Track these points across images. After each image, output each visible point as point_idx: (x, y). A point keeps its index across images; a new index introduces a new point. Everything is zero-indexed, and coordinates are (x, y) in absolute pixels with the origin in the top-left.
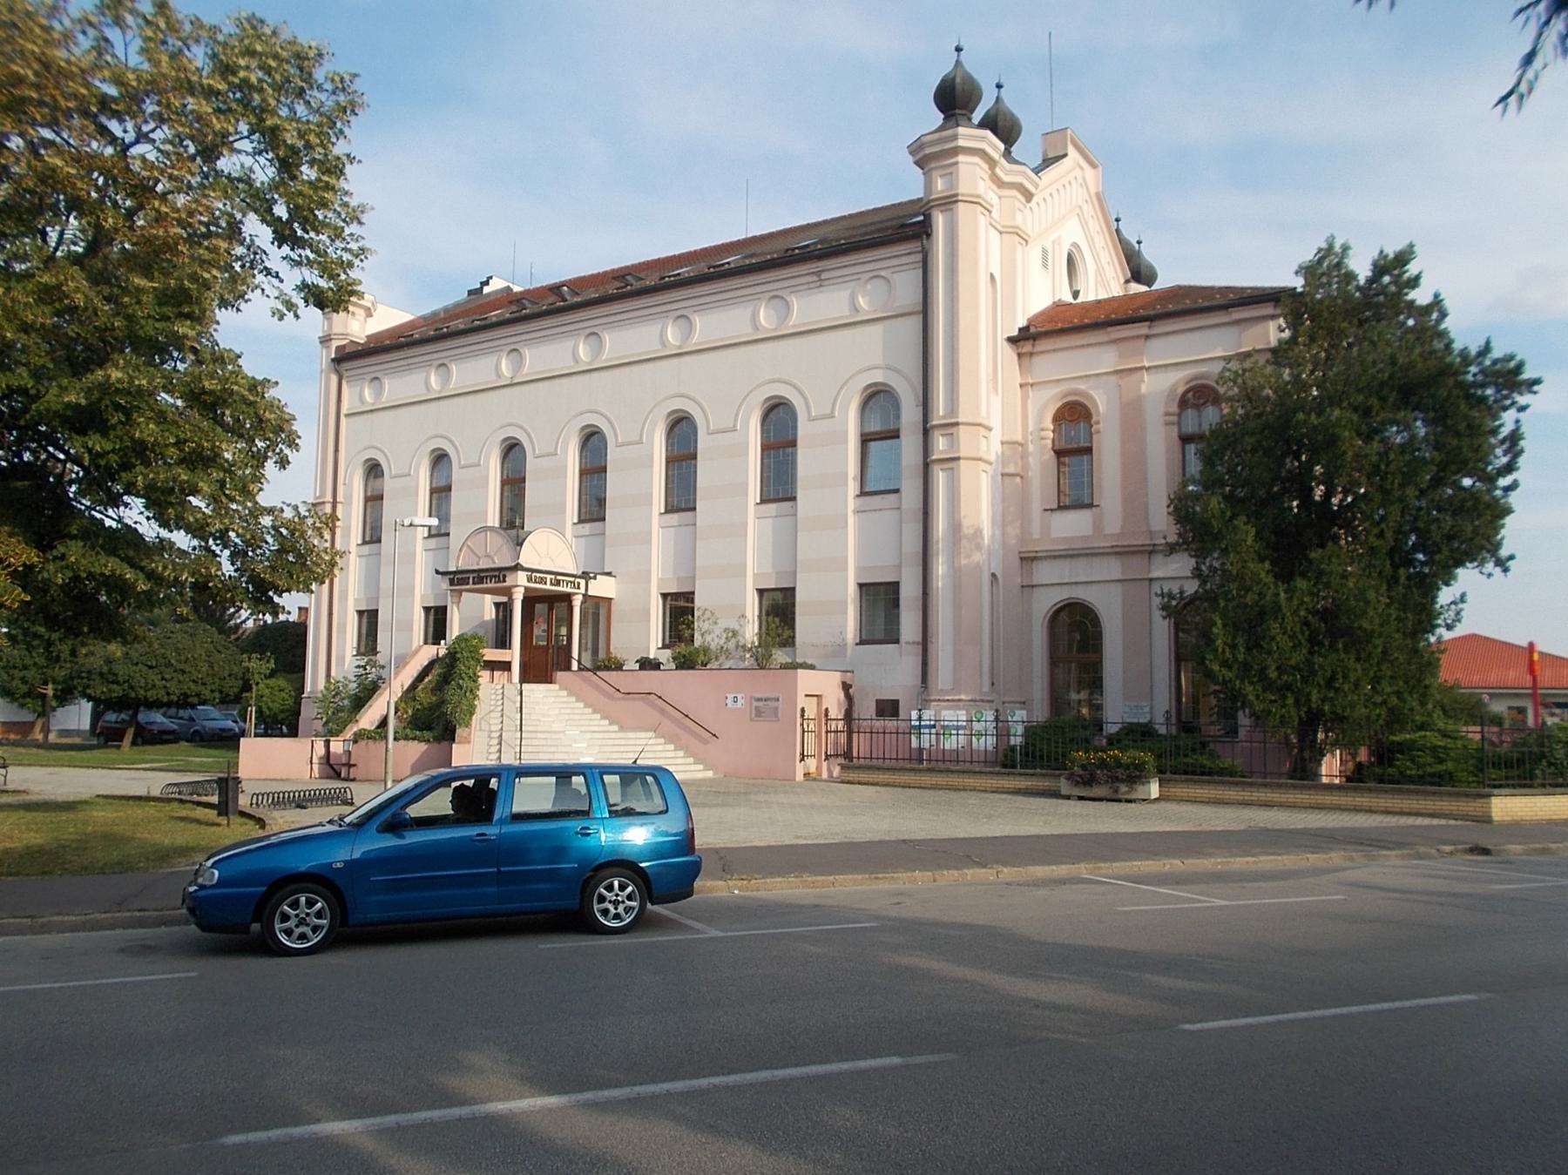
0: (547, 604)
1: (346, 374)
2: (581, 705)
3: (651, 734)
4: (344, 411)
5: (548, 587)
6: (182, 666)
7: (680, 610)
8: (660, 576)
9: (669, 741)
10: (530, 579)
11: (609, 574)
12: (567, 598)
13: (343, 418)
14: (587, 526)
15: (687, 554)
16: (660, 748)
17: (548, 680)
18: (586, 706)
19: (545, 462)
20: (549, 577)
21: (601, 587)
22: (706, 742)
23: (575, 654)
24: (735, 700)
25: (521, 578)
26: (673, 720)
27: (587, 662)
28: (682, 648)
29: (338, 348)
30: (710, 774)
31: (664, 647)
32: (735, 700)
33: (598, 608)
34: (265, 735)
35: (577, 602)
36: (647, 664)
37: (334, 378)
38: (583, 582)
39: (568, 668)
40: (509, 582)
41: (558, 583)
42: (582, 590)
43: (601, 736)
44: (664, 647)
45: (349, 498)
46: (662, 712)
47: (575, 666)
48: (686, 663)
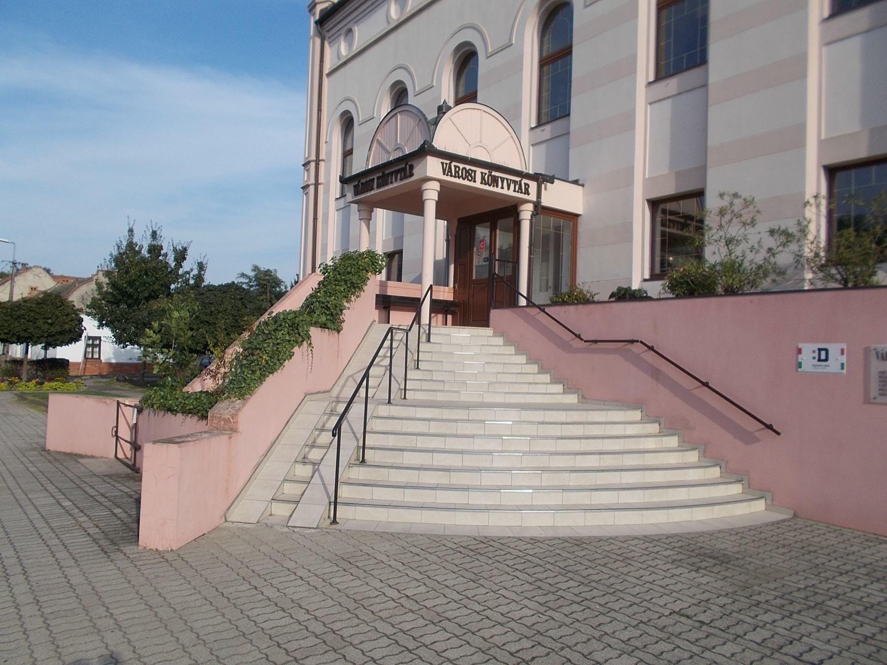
0: (477, 215)
1: (328, 35)
2: (522, 359)
3: (636, 415)
4: (326, 70)
5: (478, 184)
6: (206, 318)
7: (678, 223)
8: (646, 164)
9: (670, 426)
10: (446, 171)
11: (576, 182)
12: (508, 212)
13: (325, 77)
14: (548, 128)
15: (691, 137)
16: (650, 444)
17: (483, 321)
18: (530, 361)
19: (498, 59)
20: (479, 171)
21: (560, 196)
22: (748, 438)
23: (523, 289)
24: (823, 356)
25: (433, 167)
26: (674, 387)
27: (541, 298)
28: (684, 266)
29: (321, 11)
30: (759, 506)
31: (654, 277)
32: (823, 356)
33: (559, 228)
34: (542, 373)
35: (526, 212)
36: (624, 295)
37: (318, 41)
38: (533, 185)
39: (512, 303)
40: (417, 174)
41: (495, 181)
42: (533, 197)
43: (538, 416)
44: (654, 277)
45: (329, 154)
46: (656, 374)
47: (523, 302)
48: (693, 287)
